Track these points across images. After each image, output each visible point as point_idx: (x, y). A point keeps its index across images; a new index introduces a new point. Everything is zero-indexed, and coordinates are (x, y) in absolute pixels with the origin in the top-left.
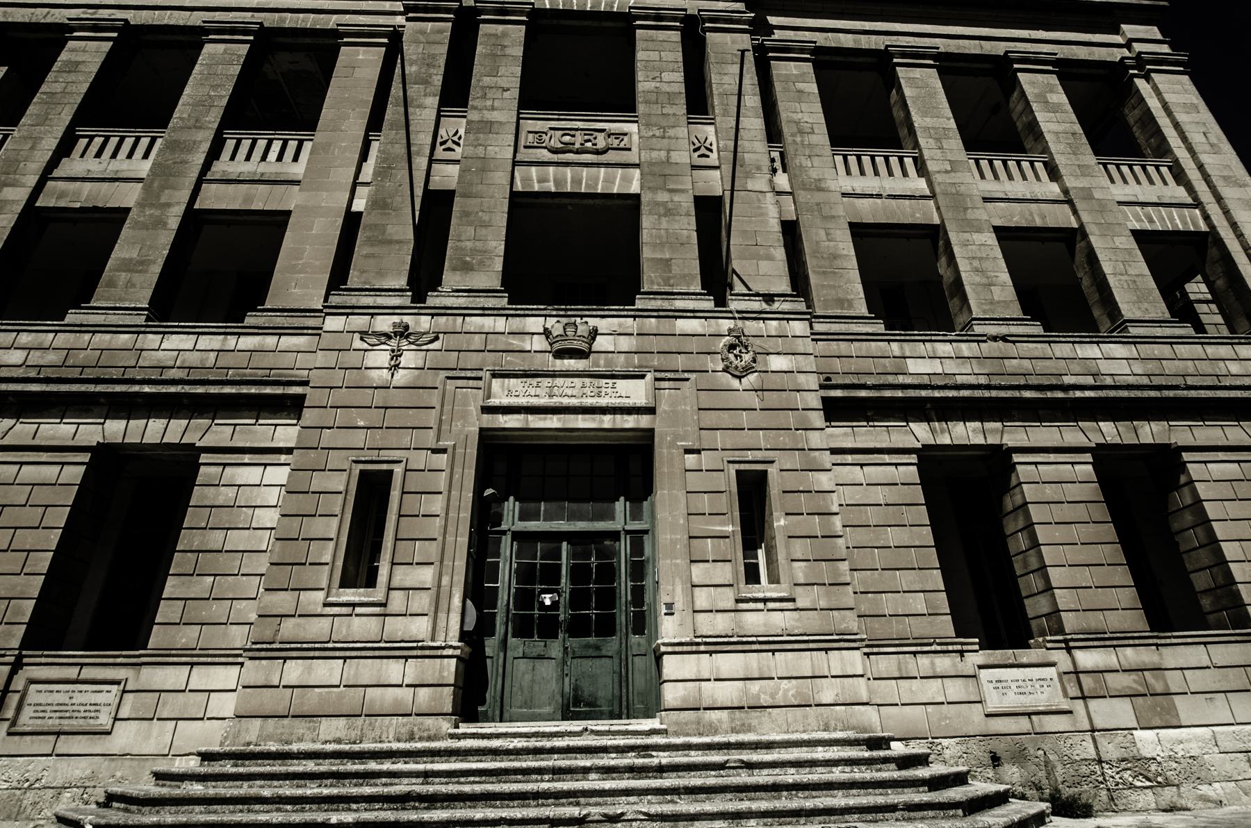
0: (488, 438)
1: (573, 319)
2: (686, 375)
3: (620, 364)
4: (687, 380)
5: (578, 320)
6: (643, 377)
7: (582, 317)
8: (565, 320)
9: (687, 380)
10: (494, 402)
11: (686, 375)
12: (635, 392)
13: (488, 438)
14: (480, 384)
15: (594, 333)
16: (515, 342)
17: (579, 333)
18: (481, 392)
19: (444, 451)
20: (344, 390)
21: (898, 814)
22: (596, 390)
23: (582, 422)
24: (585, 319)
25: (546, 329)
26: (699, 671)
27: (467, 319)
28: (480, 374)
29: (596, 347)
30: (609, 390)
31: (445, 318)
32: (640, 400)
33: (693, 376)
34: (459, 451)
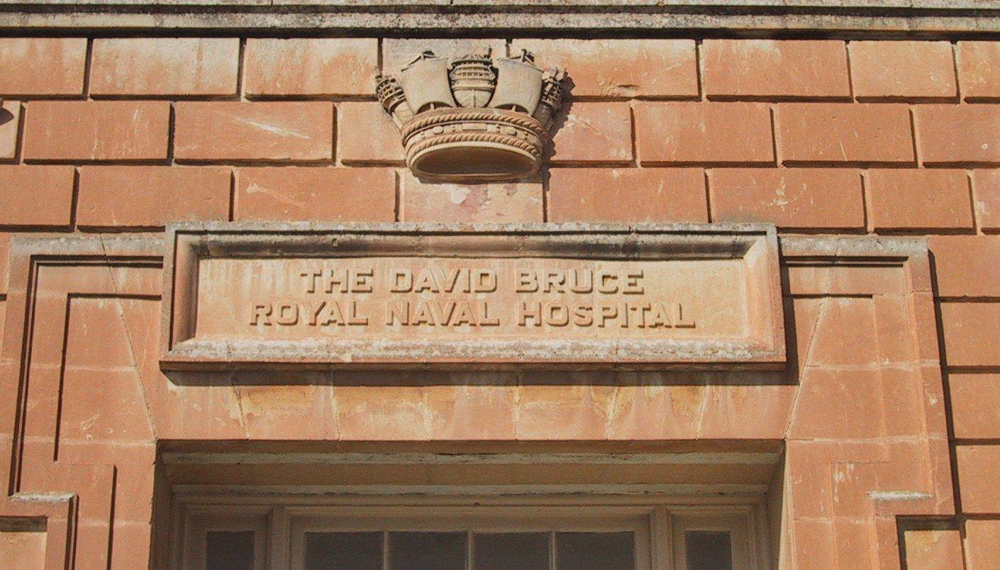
0: (184, 470)
1: (479, 47)
2: (892, 246)
3: (658, 207)
4: (896, 261)
5: (499, 45)
6: (737, 251)
7: (509, 34)
8: (449, 50)
9: (896, 261)
10: (207, 345)
11: (892, 246)
12: (724, 307)
13: (184, 470)
14: (156, 280)
15: (558, 98)
16: (274, 130)
17: (501, 97)
18: (159, 310)
19: (37, 523)
20: (922, 172)
21: (520, 497)
22: (573, 302)
23: (529, 416)
24: (518, 45)
25: (384, 82)
26: (197, 86)
27: (101, 45)
28: (159, 244)
29: (566, 142)
30: (618, 302)
31: (22, 43)
32: (746, 331)
33: (915, 248)
34: (92, 523)
